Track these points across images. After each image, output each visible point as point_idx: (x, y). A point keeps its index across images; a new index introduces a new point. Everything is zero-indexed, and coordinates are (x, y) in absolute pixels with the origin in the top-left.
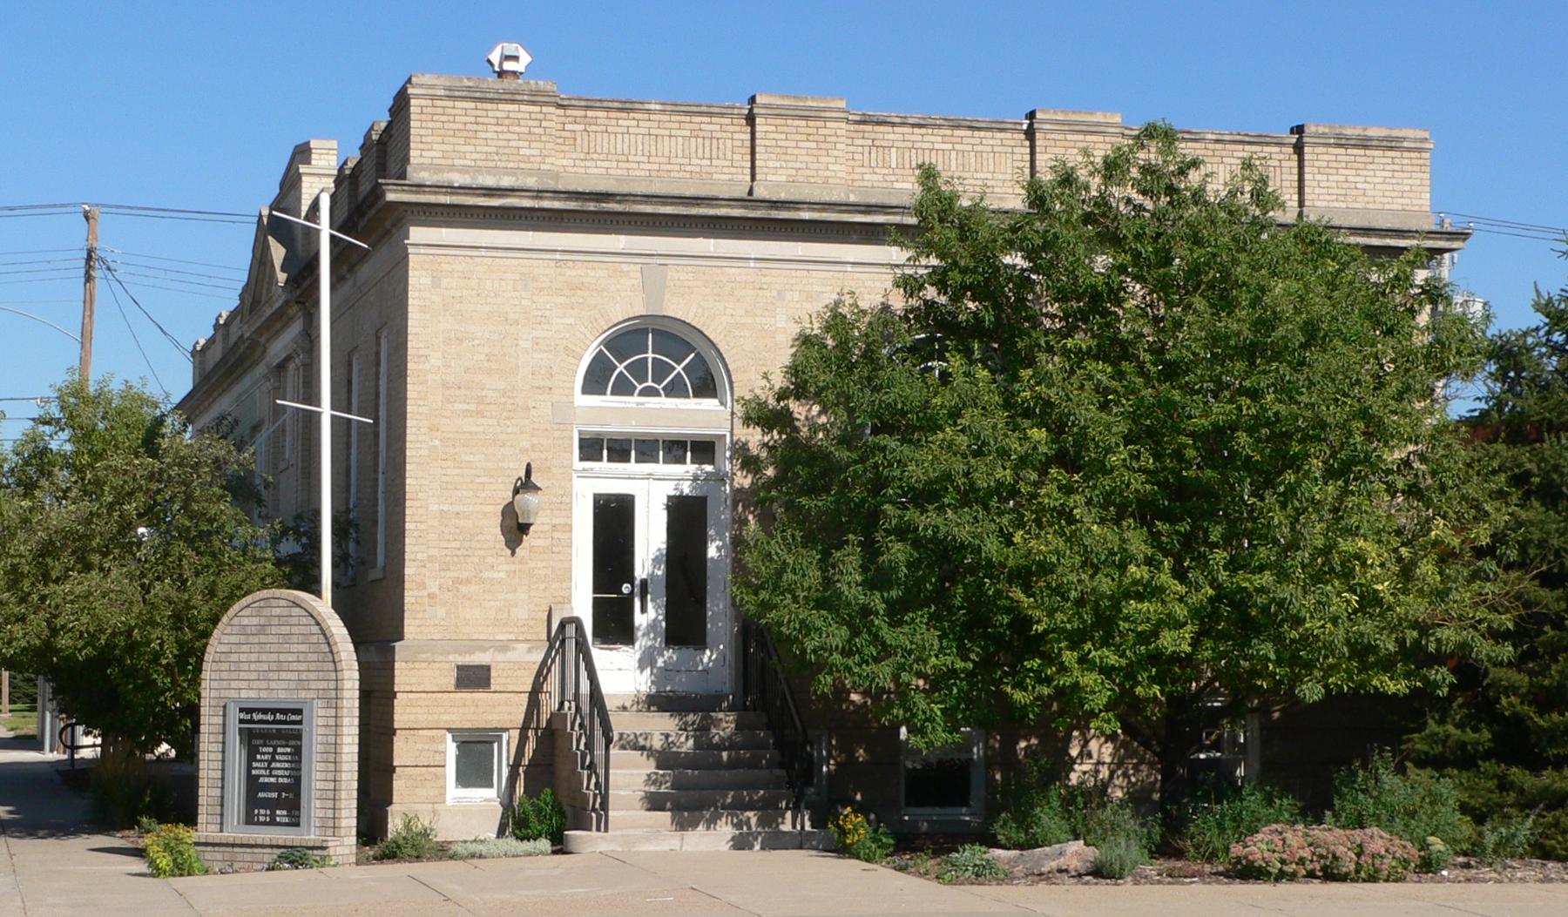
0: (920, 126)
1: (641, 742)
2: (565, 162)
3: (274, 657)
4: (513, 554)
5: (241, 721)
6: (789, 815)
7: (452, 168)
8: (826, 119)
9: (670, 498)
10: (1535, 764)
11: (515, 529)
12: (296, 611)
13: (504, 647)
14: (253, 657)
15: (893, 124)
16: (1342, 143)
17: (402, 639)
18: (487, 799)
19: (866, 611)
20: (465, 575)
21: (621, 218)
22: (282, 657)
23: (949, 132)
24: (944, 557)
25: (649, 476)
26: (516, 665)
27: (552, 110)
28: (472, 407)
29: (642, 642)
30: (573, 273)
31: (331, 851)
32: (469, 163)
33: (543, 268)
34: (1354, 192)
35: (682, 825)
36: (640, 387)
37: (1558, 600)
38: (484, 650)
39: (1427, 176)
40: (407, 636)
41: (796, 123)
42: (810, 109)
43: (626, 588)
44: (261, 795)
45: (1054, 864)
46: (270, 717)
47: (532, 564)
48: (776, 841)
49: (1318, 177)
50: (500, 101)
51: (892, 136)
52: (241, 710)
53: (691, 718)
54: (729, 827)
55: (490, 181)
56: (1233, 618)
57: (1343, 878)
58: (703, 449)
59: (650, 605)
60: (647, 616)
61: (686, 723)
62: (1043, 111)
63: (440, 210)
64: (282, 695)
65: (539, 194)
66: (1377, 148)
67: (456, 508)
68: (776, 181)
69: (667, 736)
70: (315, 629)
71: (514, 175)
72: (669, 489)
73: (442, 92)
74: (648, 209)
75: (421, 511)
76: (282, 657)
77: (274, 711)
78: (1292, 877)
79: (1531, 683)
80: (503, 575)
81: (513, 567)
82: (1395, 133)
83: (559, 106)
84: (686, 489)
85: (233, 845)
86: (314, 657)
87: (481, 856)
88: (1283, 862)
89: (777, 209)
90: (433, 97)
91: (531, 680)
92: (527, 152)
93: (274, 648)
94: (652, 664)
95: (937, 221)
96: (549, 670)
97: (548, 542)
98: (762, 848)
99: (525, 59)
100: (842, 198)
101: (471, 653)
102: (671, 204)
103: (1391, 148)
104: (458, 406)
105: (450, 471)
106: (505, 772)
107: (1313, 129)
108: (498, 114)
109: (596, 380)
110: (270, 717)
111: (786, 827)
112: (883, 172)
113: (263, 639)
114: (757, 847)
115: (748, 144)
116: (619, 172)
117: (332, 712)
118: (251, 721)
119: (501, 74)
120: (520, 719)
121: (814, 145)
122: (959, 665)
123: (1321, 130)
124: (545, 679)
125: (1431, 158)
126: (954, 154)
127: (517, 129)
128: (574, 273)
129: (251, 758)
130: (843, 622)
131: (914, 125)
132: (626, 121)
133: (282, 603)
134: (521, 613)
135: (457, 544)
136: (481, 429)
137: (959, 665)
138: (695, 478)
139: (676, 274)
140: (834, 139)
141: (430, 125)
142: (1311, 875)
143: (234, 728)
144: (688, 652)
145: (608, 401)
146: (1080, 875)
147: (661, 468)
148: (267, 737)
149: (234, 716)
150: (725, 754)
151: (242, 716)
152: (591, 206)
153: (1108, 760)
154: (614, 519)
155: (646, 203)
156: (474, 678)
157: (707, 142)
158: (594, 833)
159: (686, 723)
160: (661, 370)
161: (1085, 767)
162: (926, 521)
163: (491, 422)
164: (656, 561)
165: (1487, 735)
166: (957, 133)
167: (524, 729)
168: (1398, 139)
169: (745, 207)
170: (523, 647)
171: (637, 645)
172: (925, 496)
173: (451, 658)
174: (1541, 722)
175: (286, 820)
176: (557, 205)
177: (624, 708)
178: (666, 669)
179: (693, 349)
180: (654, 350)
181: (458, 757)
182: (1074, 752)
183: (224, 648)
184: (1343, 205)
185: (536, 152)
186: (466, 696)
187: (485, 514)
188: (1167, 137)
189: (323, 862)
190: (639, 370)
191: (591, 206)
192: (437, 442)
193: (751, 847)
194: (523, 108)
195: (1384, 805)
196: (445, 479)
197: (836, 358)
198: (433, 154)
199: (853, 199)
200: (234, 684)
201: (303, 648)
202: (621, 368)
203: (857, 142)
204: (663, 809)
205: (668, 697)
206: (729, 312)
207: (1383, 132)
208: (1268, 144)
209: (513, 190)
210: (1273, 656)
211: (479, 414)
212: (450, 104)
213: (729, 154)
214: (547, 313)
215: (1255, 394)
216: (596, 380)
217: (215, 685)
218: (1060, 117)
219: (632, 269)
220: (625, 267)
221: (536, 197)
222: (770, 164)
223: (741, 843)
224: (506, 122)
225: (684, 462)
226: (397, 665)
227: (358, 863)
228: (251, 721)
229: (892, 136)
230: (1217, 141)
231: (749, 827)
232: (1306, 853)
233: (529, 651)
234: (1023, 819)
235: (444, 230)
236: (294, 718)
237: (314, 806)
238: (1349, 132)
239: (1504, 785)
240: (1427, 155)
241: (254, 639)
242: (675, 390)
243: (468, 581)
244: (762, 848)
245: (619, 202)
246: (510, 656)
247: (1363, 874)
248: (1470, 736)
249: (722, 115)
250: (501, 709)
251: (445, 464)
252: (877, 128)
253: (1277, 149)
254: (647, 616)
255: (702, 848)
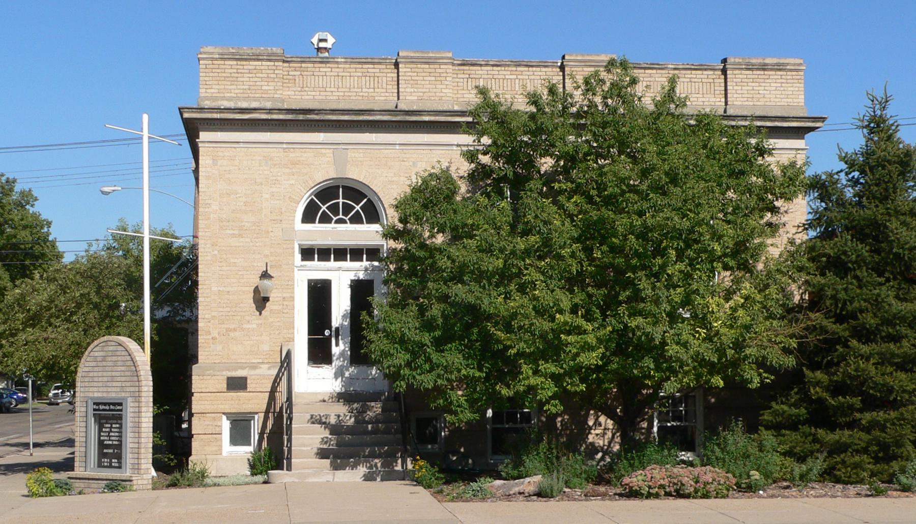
0: (497, 66)
1: (324, 420)
2: (289, 93)
3: (109, 374)
4: (260, 314)
5: (94, 410)
6: (400, 461)
7: (223, 98)
8: (440, 64)
9: (352, 281)
10: (832, 427)
11: (261, 301)
12: (120, 348)
13: (254, 367)
14: (100, 374)
15: (481, 65)
16: (750, 67)
17: (197, 362)
18: (246, 451)
19: (422, 345)
20: (232, 327)
21: (320, 124)
22: (114, 374)
23: (514, 69)
24: (474, 314)
25: (339, 269)
26: (261, 378)
27: (281, 64)
28: (236, 232)
29: (336, 363)
30: (294, 155)
31: (135, 482)
32: (233, 95)
33: (275, 153)
34: (758, 96)
35: (335, 467)
36: (335, 219)
37: (844, 330)
38: (243, 368)
39: (802, 85)
40: (200, 361)
41: (423, 66)
42: (430, 58)
43: (327, 333)
44: (105, 451)
45: (517, 489)
46: (107, 408)
47: (271, 320)
48: (390, 476)
49: (736, 88)
50: (250, 60)
51: (480, 72)
52: (94, 404)
53: (355, 406)
54: (365, 469)
55: (244, 105)
56: (624, 345)
57: (687, 496)
58: (373, 253)
59: (341, 342)
60: (339, 348)
61: (352, 409)
62: (571, 55)
63: (216, 122)
64: (113, 395)
65: (270, 111)
66: (771, 70)
67: (228, 289)
68: (411, 99)
69: (339, 416)
70: (128, 358)
71: (259, 101)
72: (351, 276)
73: (217, 56)
74: (334, 118)
75: (207, 291)
76: (114, 374)
77: (109, 404)
78: (657, 496)
79: (830, 380)
80: (255, 326)
81: (260, 322)
82: (782, 61)
83: (284, 61)
84: (361, 275)
85: (89, 479)
86: (128, 374)
87: (219, 485)
88: (650, 487)
89: (409, 115)
90: (213, 59)
91: (270, 385)
92: (267, 88)
93: (110, 369)
94: (342, 375)
95: (488, 117)
96: (281, 379)
97: (281, 307)
98: (382, 480)
99: (331, 40)
100: (450, 108)
101: (236, 369)
102: (347, 114)
103: (780, 70)
104: (228, 232)
105: (224, 268)
106: (257, 437)
107: (732, 60)
108: (250, 67)
109: (310, 215)
110: (107, 408)
111: (399, 468)
112: (452, 91)
113: (104, 364)
114: (379, 479)
115: (396, 79)
116: (321, 97)
117: (137, 404)
118: (99, 410)
119: (319, 49)
120: (264, 407)
121: (433, 78)
122: (477, 374)
123: (737, 60)
124: (278, 384)
125: (805, 75)
126: (517, 81)
127: (261, 75)
128: (294, 155)
129: (100, 431)
130: (407, 350)
131: (493, 66)
132: (324, 69)
133: (113, 343)
134: (266, 347)
135: (229, 309)
136: (241, 244)
137: (477, 374)
138: (366, 269)
139: (353, 154)
140: (445, 75)
141: (211, 74)
142: (668, 494)
143: (91, 412)
144: (363, 368)
145: (317, 227)
146: (530, 496)
147: (348, 264)
148: (108, 419)
149: (91, 407)
150: (370, 426)
151: (95, 407)
152: (301, 117)
153: (611, 427)
154: (320, 294)
155: (332, 114)
156: (237, 384)
157: (372, 79)
158: (285, 472)
159: (352, 409)
160: (347, 209)
161: (598, 432)
162: (459, 291)
163: (247, 240)
164: (344, 317)
165: (803, 411)
166: (519, 69)
167: (267, 412)
168: (783, 64)
169: (390, 115)
170: (265, 366)
171: (333, 364)
172: (457, 277)
173: (224, 373)
174: (833, 402)
175: (117, 465)
176: (281, 117)
177: (324, 401)
178: (351, 378)
179: (365, 196)
180: (339, 198)
181: (231, 429)
182: (591, 423)
183: (86, 369)
184: (751, 103)
185: (272, 88)
186: (233, 394)
187: (244, 292)
188: (624, 65)
189: (125, 489)
190: (334, 209)
191: (301, 117)
192: (216, 252)
193: (375, 480)
194: (264, 63)
195: (728, 453)
196: (221, 273)
197: (430, 196)
198: (212, 91)
199: (456, 108)
200: (91, 389)
201: (123, 369)
202: (324, 208)
203: (460, 76)
204: (328, 458)
205: (351, 394)
206: (385, 175)
207: (775, 61)
208: (706, 70)
209: (255, 109)
210: (652, 366)
211: (240, 235)
212: (222, 62)
213: (384, 85)
214: (279, 178)
215: (641, 214)
216: (310, 215)
217: (82, 389)
218: (579, 58)
219: (328, 152)
220: (323, 151)
221: (269, 113)
222: (408, 90)
223: (369, 478)
224: (255, 71)
225: (362, 260)
226: (193, 377)
227: (153, 489)
228: (99, 410)
229: (480, 72)
230: (675, 69)
231: (377, 468)
232: (665, 482)
233: (269, 368)
234: (518, 464)
235: (219, 133)
236: (119, 408)
237: (129, 457)
238: (754, 61)
239: (815, 440)
240: (802, 73)
241: (100, 364)
242: (356, 219)
243: (235, 330)
244: (382, 480)
245: (317, 114)
246: (258, 371)
247: (699, 494)
248: (795, 411)
249: (380, 63)
250: (253, 402)
251: (221, 264)
252: (472, 68)
253: (712, 72)
254: (339, 348)
255: (346, 480)
